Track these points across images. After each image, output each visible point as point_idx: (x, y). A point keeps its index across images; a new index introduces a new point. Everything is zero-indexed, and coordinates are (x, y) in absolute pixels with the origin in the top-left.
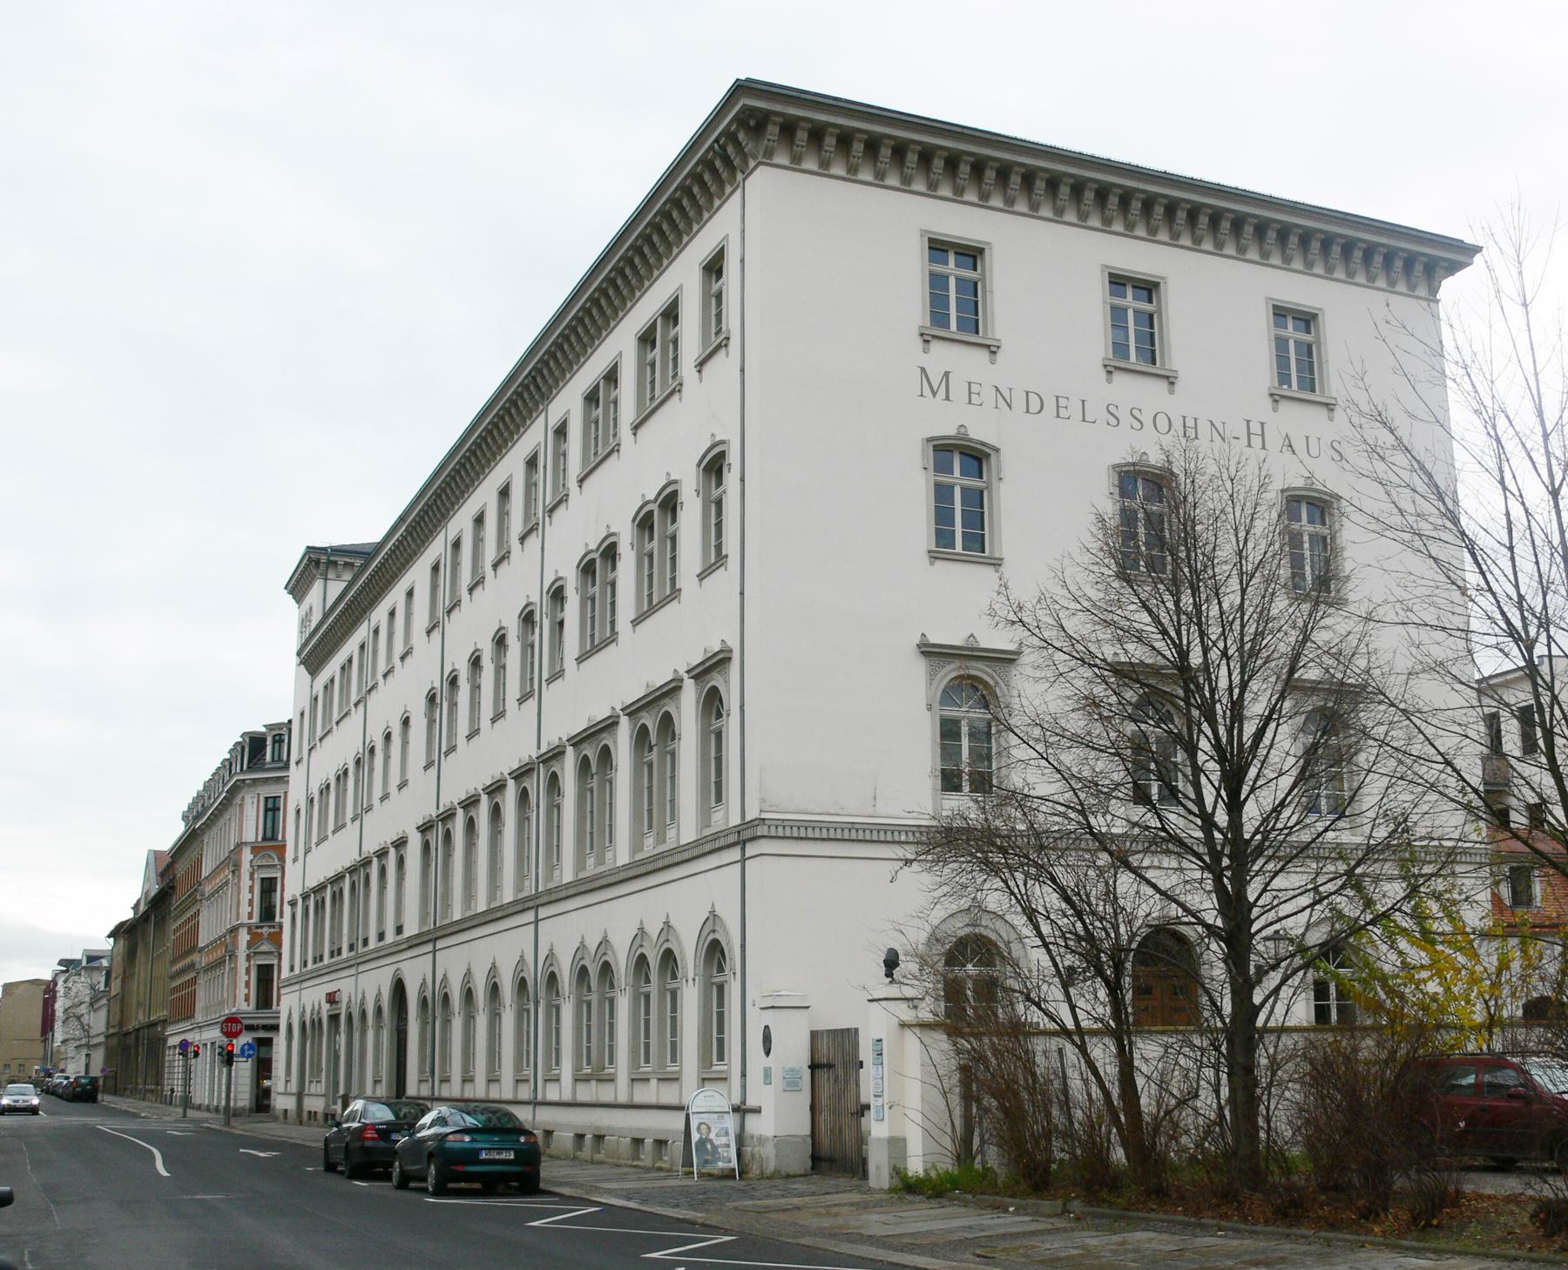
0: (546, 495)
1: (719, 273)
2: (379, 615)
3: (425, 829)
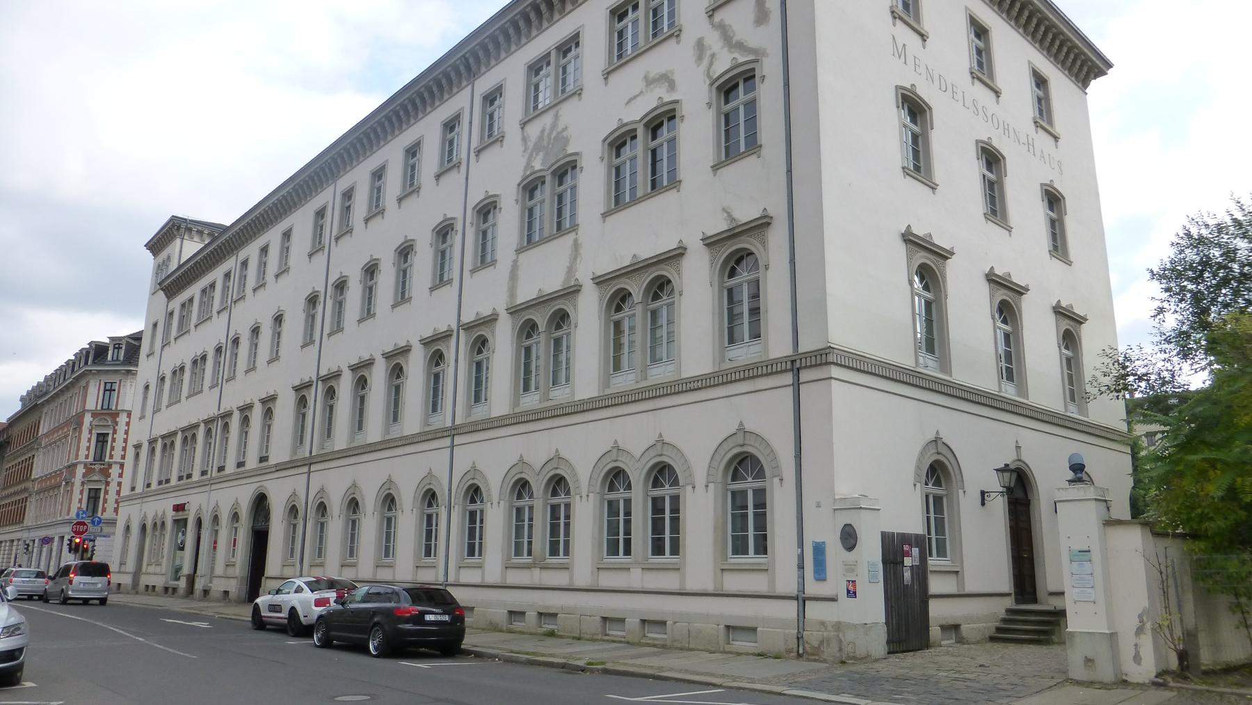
1: (323, 216)
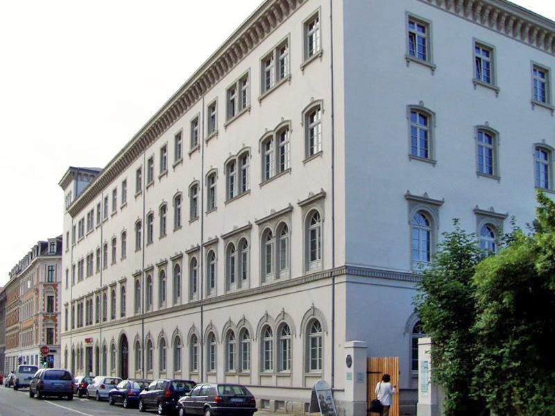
3: (136, 275)
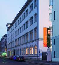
0: (23, 18)
2: (12, 27)
3: (15, 40)
